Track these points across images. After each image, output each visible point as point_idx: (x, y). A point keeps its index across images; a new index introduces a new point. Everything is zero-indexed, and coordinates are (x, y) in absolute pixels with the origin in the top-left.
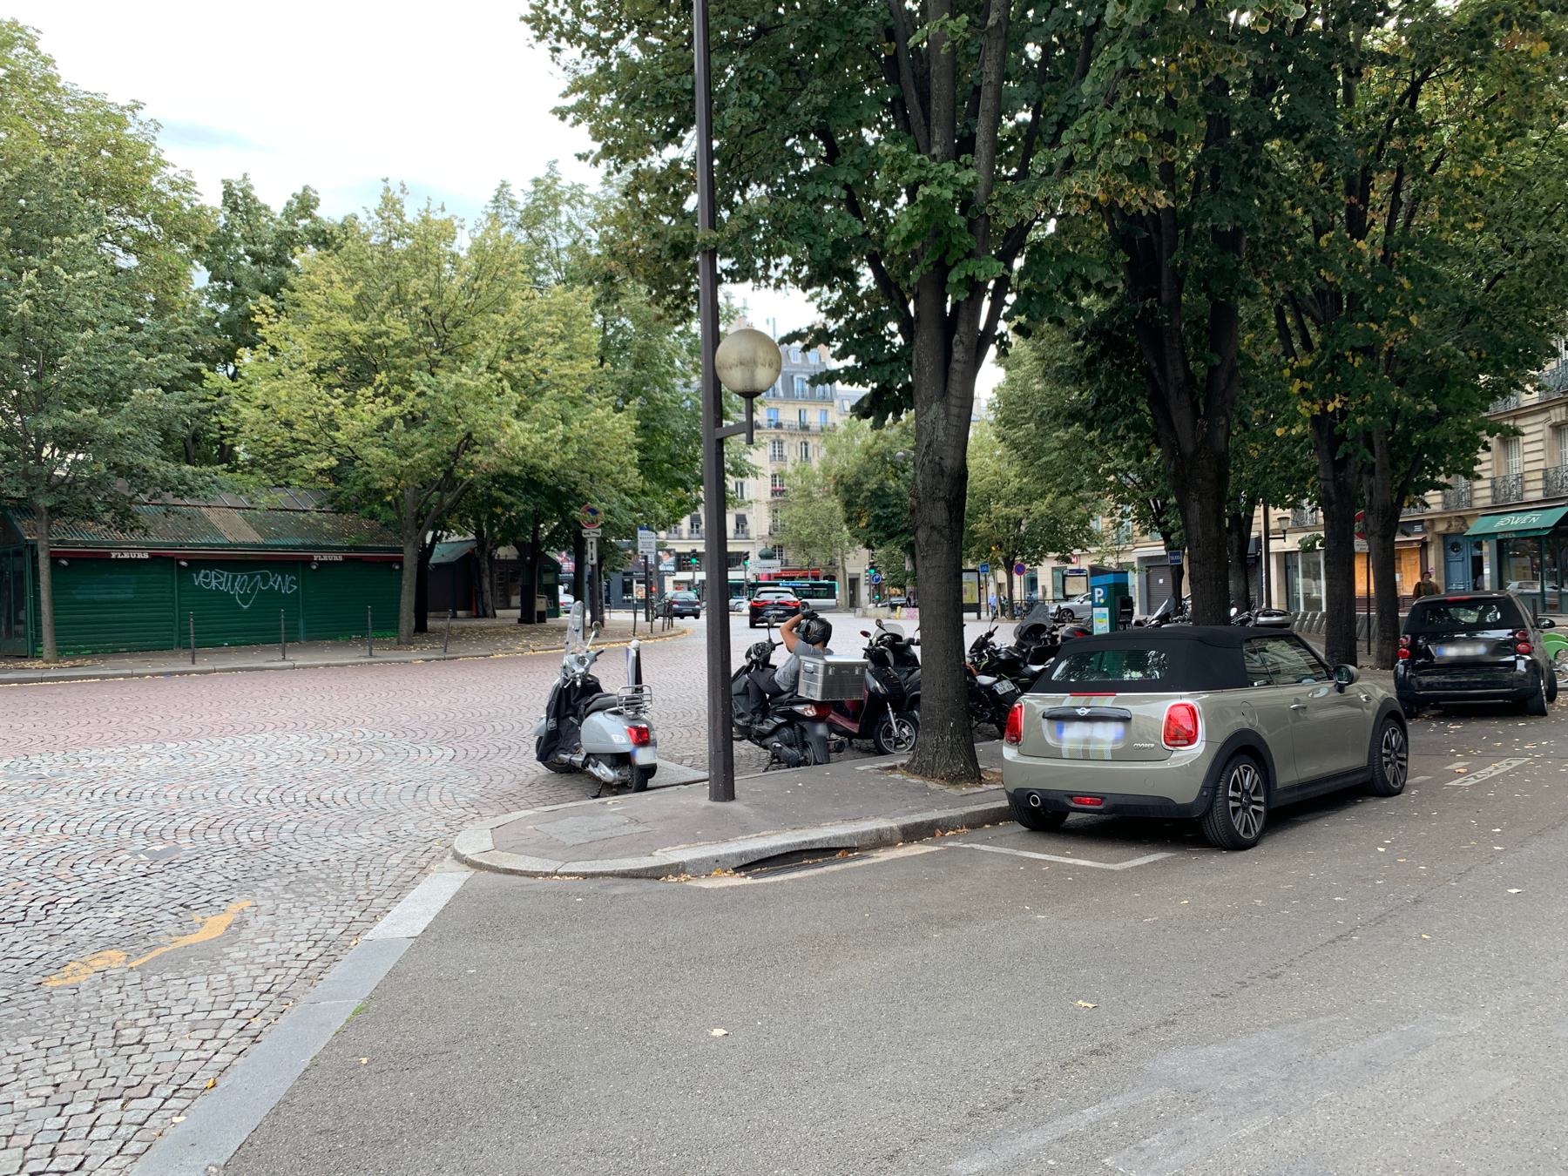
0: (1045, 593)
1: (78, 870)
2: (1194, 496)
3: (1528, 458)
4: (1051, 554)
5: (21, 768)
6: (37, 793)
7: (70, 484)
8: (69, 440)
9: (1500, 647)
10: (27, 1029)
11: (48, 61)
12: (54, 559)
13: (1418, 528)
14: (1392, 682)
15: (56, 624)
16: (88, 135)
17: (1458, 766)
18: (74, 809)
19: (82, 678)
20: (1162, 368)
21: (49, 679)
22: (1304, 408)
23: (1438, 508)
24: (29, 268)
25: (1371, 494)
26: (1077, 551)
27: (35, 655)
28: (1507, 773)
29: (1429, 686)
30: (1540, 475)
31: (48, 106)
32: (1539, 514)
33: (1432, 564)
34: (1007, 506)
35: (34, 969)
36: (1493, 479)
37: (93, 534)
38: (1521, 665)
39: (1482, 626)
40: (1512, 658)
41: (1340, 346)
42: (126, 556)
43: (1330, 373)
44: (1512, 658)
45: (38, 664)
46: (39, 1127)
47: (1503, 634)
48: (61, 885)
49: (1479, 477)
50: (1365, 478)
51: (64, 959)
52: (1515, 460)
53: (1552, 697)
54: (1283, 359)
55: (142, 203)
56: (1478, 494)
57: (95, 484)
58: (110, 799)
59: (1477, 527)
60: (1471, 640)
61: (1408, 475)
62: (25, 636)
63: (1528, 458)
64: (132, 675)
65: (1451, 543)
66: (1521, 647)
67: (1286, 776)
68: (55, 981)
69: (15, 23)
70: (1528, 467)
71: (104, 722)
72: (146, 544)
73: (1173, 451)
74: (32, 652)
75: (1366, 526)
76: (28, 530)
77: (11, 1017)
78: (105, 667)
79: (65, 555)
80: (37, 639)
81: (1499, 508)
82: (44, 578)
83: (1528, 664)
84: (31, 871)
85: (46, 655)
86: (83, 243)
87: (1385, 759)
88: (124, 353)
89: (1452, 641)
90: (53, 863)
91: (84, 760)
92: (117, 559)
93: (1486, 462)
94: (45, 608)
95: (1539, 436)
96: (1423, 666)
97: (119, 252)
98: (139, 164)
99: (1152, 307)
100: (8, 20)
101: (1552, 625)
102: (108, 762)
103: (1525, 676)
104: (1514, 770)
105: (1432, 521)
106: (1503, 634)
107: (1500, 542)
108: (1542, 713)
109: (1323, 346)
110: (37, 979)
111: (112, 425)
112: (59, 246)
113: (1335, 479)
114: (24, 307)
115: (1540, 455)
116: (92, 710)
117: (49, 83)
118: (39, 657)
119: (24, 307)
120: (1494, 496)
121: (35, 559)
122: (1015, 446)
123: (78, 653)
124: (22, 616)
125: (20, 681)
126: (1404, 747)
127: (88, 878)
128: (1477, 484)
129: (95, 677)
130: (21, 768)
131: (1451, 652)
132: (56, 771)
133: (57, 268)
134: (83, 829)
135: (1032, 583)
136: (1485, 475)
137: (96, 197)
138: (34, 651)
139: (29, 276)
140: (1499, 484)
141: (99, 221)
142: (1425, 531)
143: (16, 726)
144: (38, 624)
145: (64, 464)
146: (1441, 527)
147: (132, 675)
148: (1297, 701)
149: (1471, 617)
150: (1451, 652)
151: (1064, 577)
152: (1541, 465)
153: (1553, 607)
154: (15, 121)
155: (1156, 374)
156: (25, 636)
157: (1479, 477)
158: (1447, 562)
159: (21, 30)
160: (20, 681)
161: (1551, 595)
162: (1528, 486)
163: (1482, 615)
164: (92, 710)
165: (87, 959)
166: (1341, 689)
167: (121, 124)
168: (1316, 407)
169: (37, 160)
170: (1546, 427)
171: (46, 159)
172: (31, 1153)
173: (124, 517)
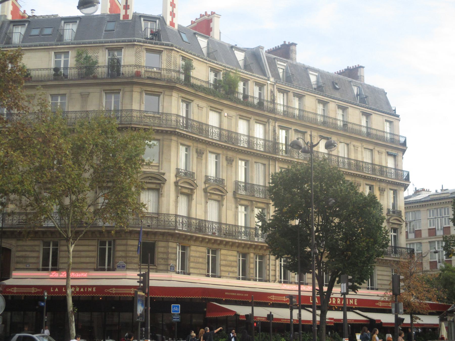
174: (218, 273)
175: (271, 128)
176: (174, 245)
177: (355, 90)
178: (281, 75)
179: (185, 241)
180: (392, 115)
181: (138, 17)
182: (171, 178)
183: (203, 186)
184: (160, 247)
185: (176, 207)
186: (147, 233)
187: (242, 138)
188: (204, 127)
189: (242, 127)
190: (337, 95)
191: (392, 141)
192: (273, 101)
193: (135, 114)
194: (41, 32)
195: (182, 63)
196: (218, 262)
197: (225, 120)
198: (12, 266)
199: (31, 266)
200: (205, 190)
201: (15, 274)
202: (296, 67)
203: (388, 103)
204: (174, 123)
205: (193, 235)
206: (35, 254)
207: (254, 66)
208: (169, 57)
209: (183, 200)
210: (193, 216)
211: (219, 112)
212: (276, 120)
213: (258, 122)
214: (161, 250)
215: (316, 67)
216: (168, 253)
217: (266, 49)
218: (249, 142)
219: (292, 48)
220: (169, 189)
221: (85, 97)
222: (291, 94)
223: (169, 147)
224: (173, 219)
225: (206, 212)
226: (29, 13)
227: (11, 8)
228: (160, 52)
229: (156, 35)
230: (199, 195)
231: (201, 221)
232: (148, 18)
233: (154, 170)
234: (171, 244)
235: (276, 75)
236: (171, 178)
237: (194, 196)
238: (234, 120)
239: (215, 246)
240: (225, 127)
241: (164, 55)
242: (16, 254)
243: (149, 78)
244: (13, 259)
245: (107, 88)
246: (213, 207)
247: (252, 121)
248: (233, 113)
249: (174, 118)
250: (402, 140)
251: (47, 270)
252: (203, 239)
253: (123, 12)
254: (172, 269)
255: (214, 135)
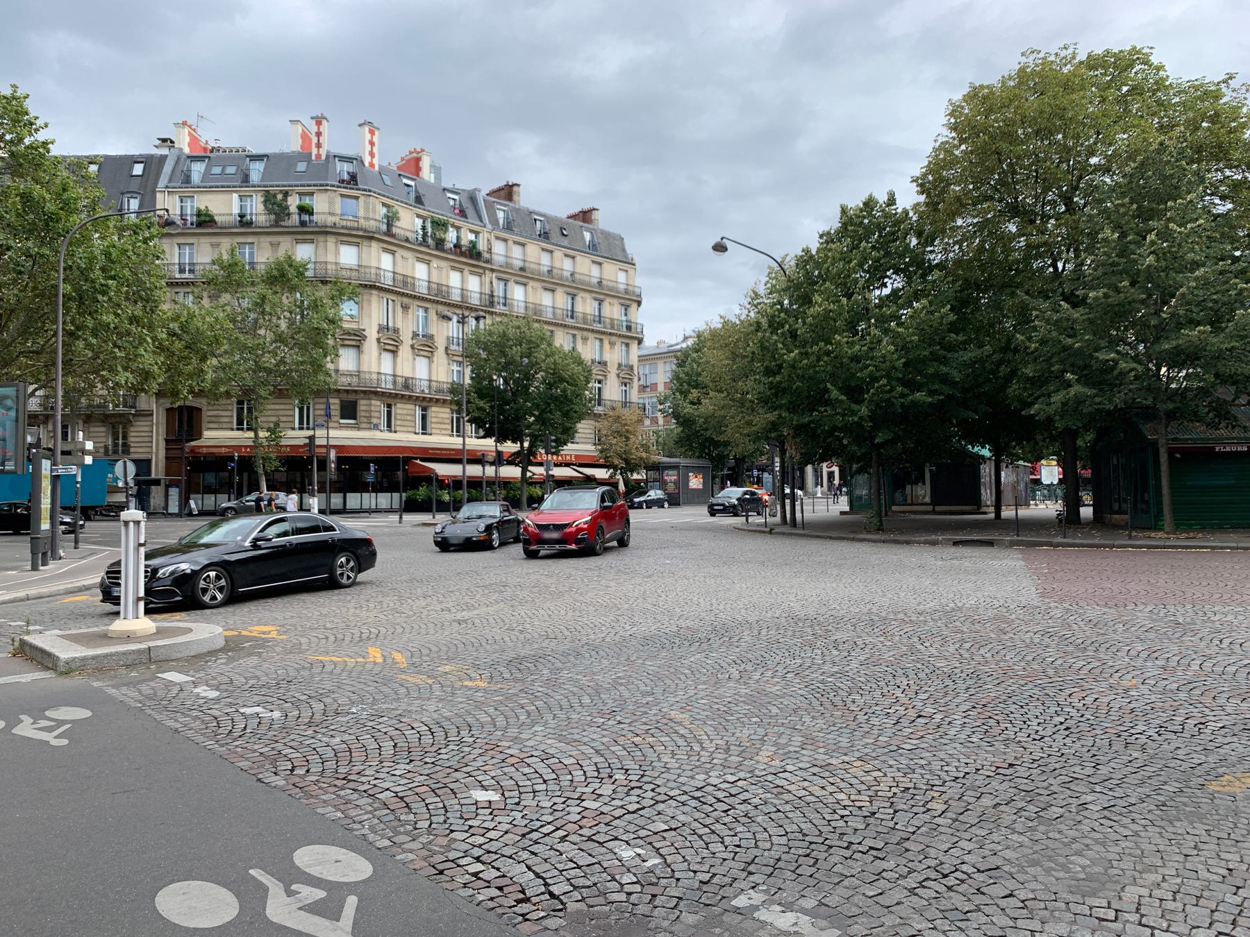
1: (1221, 701)
5: (1161, 614)
6: (1177, 635)
7: (1182, 394)
8: (1178, 359)
10: (1201, 818)
11: (1159, 68)
12: (1171, 452)
15: (1173, 503)
16: (1191, 115)
18: (1208, 652)
19: (1196, 547)
21: (1169, 547)
24: (1150, 231)
27: (1157, 528)
31: (1160, 103)
35: (1197, 772)
37: (1197, 433)
42: (1228, 449)
45: (1160, 534)
46: (1221, 898)
48: (1207, 711)
51: (1221, 770)
55: (1237, 155)
57: (1204, 392)
58: (1237, 648)
62: (1147, 512)
64: (1237, 548)
68: (1214, 787)
69: (1134, 48)
71: (1222, 585)
72: (1246, 438)
74: (1154, 525)
76: (1149, 431)
77: (1185, 805)
78: (1214, 540)
79: (1179, 450)
80: (1159, 515)
82: (1164, 467)
84: (1182, 695)
85: (1167, 529)
86: (1191, 201)
88: (1226, 282)
90: (1197, 692)
91: (1210, 614)
92: (1220, 452)
94: (1165, 491)
97: (1217, 201)
98: (1233, 124)
100: (1128, 48)
102: (1230, 618)
110: (1201, 781)
111: (1218, 342)
112: (1171, 208)
114: (1151, 260)
116: (1210, 574)
117: (1160, 84)
118: (1160, 530)
119: (1151, 260)
121: (1156, 454)
123: (1190, 528)
124: (1146, 498)
125: (1149, 547)
127: (1229, 710)
129: (1206, 547)
130: (1161, 614)
132: (1188, 620)
133: (1171, 225)
134: (1218, 669)
137: (1199, 161)
138: (1156, 525)
139: (1151, 237)
141: (1202, 180)
143: (1153, 581)
144: (1159, 504)
145: (1178, 378)
147: (1237, 548)
154: (1136, 122)
156: (1147, 512)
159: (1139, 52)
160: (1149, 547)
164: (1210, 574)
165: (1238, 775)
167: (1217, 96)
169: (1155, 146)
171: (1161, 144)
172: (1217, 916)
173: (1222, 413)
174: (429, 431)
175: (488, 280)
176: (378, 403)
177: (587, 236)
178: (501, 222)
179: (390, 399)
180: (627, 262)
181: (332, 157)
182: (372, 334)
183: (411, 342)
184: (363, 405)
185: (379, 364)
186: (347, 391)
187: (454, 291)
188: (409, 280)
189: (454, 279)
190: (565, 242)
191: (627, 292)
192: (490, 251)
193: (329, 267)
194: (223, 170)
195: (384, 210)
196: (429, 420)
197: (434, 272)
198: (204, 425)
199: (225, 426)
200: (412, 347)
201: (207, 434)
202: (518, 210)
203: (624, 250)
204: (373, 276)
205: (400, 395)
206: (229, 413)
207: (470, 212)
208: (367, 204)
209: (387, 357)
210: (399, 373)
211: (428, 263)
212: (492, 270)
213: (472, 273)
214: (362, 408)
215: (542, 210)
216: (370, 411)
217: (485, 190)
218: (462, 296)
219: (515, 189)
220: (371, 346)
221: (275, 246)
222: (510, 243)
223: (370, 301)
224: (375, 377)
225: (414, 369)
226: (212, 144)
227: (187, 139)
228: (357, 198)
229: (353, 178)
230: (405, 351)
231: (407, 379)
232: (344, 159)
233: (354, 326)
234: (373, 402)
235: (494, 221)
236: (372, 334)
237: (400, 353)
238: (444, 271)
239: (425, 404)
240: (435, 279)
241: (362, 199)
242: (207, 413)
243: (343, 227)
244: (205, 418)
245: (299, 237)
246: (422, 363)
247: (466, 272)
248: (443, 264)
249: (373, 271)
250: (637, 291)
251: (242, 429)
252: (410, 397)
253: (314, 151)
254: (376, 427)
255: (422, 289)
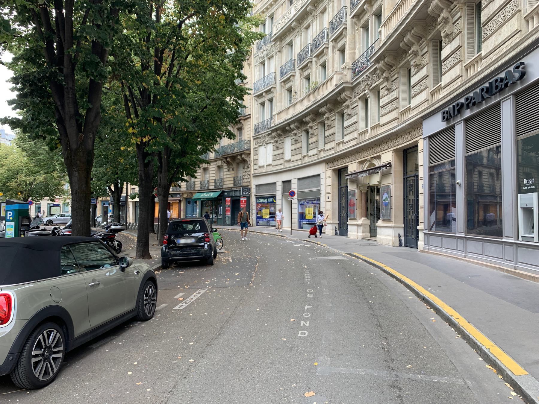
0: (44, 213)
2: (75, 169)
3: (211, 175)
4: (45, 198)
9: (199, 239)
13: (178, 196)
14: (160, 252)
17: (179, 296)
20: (63, 105)
22: (133, 140)
23: (185, 189)
25: (160, 180)
26: (57, 197)
28: (198, 298)
29: (175, 255)
30: (213, 181)
32: (213, 193)
33: (182, 207)
34: (25, 176)
36: (201, 181)
38: (206, 246)
39: (194, 231)
40: (203, 244)
41: (149, 116)
43: (144, 126)
44: (203, 244)
47: (200, 234)
49: (196, 178)
50: (159, 174)
52: (207, 176)
53: (215, 257)
54: (126, 118)
56: (196, 186)
59: (196, 196)
60: (190, 237)
61: (173, 174)
63: (211, 175)
65: (188, 201)
66: (207, 239)
67: (81, 328)
70: (211, 178)
73: (67, 148)
75: (158, 192)
81: (202, 191)
83: (208, 246)
87: (145, 303)
89: (184, 237)
93: (199, 174)
95: (214, 169)
96: (172, 247)
99: (55, 72)
101: (216, 231)
103: (207, 250)
104: (201, 296)
105: (183, 193)
106: (200, 234)
107: (202, 201)
108: (212, 264)
109: (142, 116)
113: (144, 171)
115: (214, 175)
120: (201, 187)
122: (24, 150)
126: (155, 294)
128: (196, 180)
131: (182, 241)
135: (39, 209)
136: (198, 177)
140: (202, 183)
142: (180, 196)
146: (185, 196)
148: (93, 281)
149: (190, 227)
150: (182, 241)
151: (50, 207)
152: (214, 178)
153: (215, 222)
155: (60, 108)
157: (196, 178)
158: (186, 207)
161: (215, 219)
162: (211, 184)
163: (194, 227)
166: (123, 269)
168: (138, 140)
170: (216, 166)
